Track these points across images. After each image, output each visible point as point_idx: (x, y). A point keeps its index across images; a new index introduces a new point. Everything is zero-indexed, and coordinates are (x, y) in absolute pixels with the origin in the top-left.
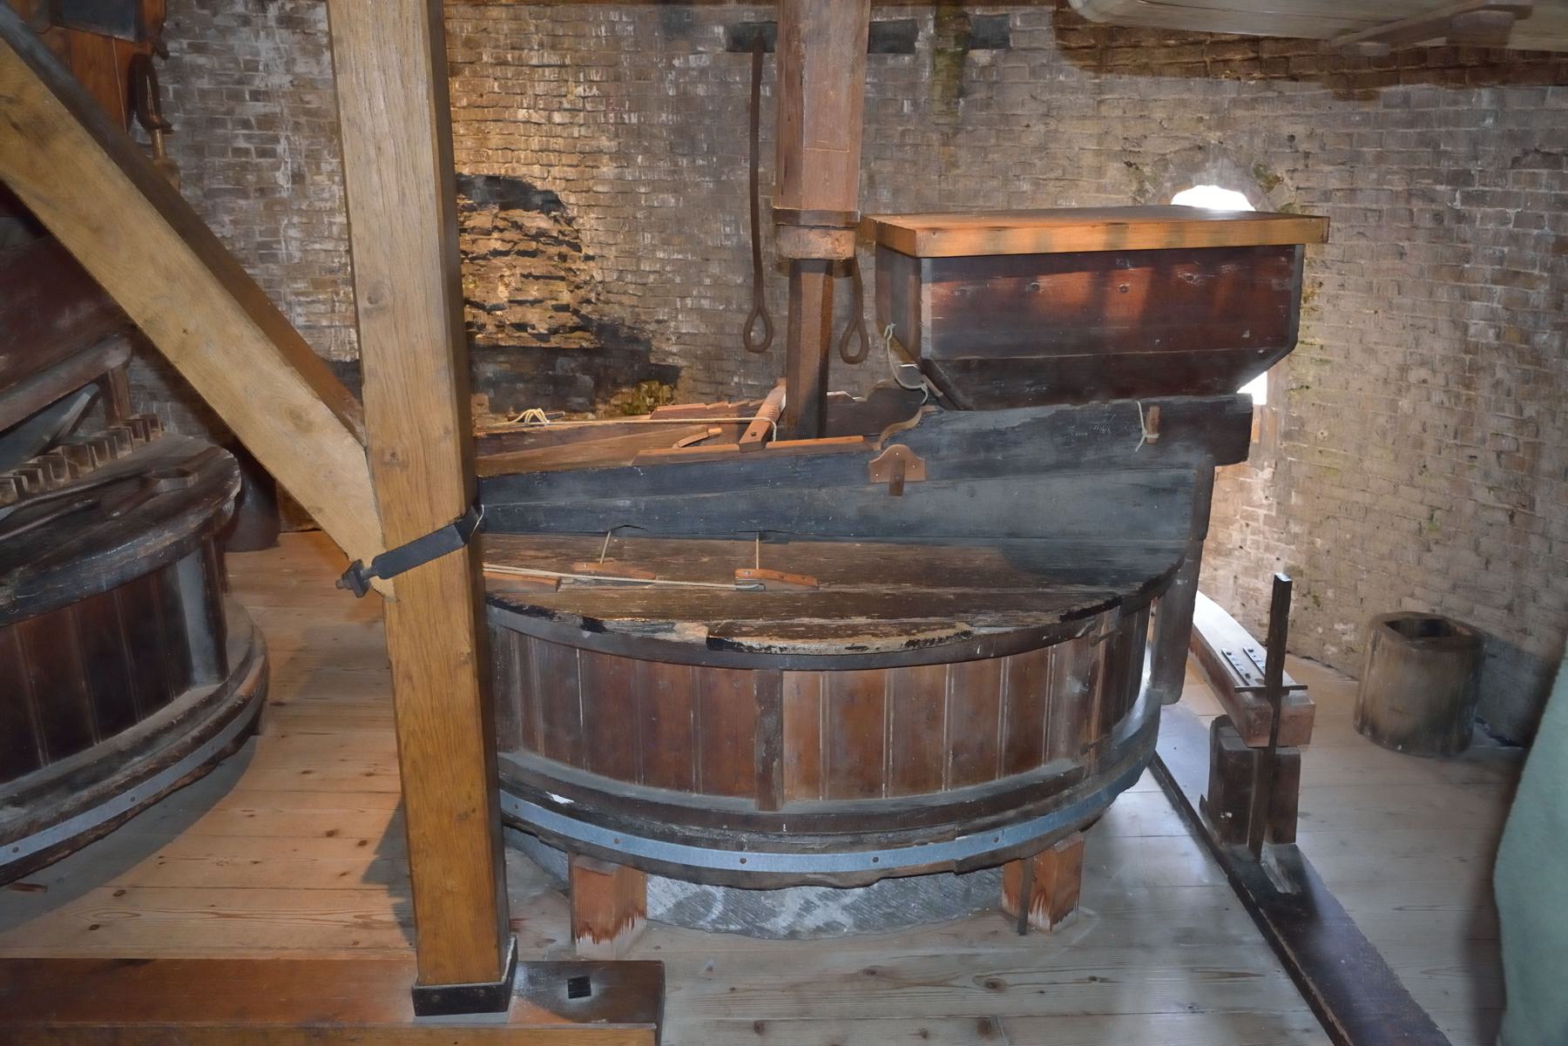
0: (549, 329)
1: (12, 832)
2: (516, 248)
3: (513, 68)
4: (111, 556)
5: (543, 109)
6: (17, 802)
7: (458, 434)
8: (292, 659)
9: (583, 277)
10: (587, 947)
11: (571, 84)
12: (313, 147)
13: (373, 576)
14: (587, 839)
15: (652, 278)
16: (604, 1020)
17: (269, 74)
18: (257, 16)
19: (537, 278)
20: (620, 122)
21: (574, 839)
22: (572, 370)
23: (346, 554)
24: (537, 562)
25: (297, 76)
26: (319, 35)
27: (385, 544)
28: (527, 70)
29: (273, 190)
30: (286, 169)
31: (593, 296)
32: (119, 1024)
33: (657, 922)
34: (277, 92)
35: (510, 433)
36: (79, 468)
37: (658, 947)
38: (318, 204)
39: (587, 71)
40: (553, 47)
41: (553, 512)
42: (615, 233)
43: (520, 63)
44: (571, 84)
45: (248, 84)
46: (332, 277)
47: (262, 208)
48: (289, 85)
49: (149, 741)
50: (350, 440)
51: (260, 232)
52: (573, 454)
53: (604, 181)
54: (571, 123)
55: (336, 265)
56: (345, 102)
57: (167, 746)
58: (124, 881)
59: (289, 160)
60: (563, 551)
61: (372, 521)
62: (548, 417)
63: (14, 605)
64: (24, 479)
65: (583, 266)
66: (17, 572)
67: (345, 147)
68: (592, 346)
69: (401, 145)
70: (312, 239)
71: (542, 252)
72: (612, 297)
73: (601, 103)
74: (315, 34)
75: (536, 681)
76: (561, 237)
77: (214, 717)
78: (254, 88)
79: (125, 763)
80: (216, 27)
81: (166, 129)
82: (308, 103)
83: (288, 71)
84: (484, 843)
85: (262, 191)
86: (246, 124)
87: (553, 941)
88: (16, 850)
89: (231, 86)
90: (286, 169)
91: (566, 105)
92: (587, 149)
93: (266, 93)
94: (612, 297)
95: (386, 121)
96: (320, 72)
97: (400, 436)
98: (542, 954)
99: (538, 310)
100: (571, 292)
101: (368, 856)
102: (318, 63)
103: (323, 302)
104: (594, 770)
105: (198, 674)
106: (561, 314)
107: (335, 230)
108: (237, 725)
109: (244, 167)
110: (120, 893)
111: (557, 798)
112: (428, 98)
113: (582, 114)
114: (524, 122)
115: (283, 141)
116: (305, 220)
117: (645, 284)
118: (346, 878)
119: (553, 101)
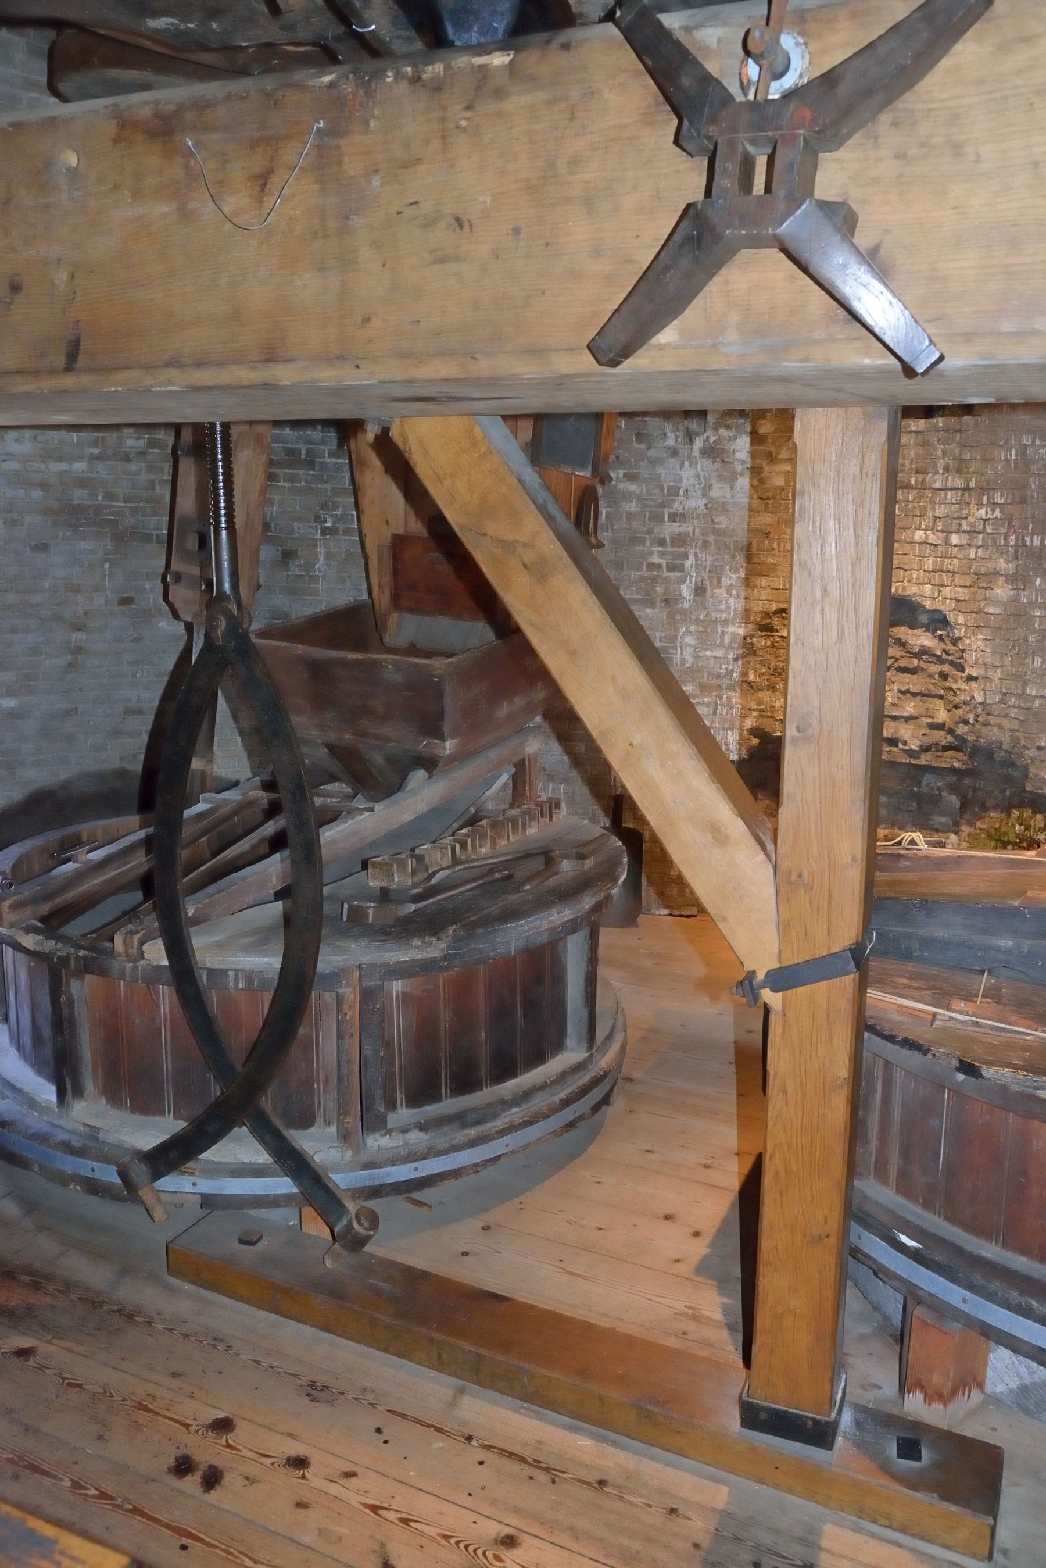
0: (921, 746)
1: (415, 1154)
2: (896, 665)
3: (915, 492)
4: (522, 926)
5: (941, 531)
6: (423, 1127)
7: (864, 863)
8: (643, 1038)
9: (963, 697)
10: (915, 1405)
11: (973, 507)
12: (716, 563)
13: (765, 987)
14: (933, 1290)
15: (1037, 703)
16: (935, 1495)
17: (687, 498)
18: (685, 448)
19: (914, 695)
20: (1021, 544)
21: (916, 1286)
22: (939, 789)
23: (742, 963)
24: (911, 992)
25: (711, 500)
26: (736, 463)
27: (780, 959)
28: (929, 493)
29: (677, 601)
30: (691, 582)
31: (971, 717)
32: (483, 1352)
33: (994, 1400)
34: (692, 514)
35: (886, 854)
36: (497, 840)
37: (994, 1429)
38: (714, 615)
39: (991, 493)
40: (959, 471)
41: (928, 943)
42: (1003, 655)
43: (923, 486)
44: (973, 507)
45: (669, 507)
46: (719, 682)
47: (665, 617)
48: (703, 507)
49: (526, 1096)
50: (762, 856)
51: (661, 638)
52: (950, 884)
53: (996, 603)
54: (968, 545)
55: (723, 671)
56: (799, 547)
57: (540, 1102)
58: (493, 1216)
59: (694, 575)
60: (938, 985)
61: (770, 936)
62: (926, 842)
63: (445, 958)
64: (458, 846)
65: (964, 686)
66: (451, 929)
67: (794, 587)
68: (964, 767)
69: (846, 589)
70: (705, 647)
71: (923, 669)
72: (992, 720)
73: (1003, 525)
74: (732, 463)
75: (897, 1114)
76: (944, 656)
77: (580, 1083)
78: (671, 511)
79: (506, 1111)
80: (649, 459)
81: (600, 545)
82: (718, 524)
83: (704, 495)
84: (833, 1272)
85: (667, 601)
86: (662, 542)
87: (880, 1388)
88: (416, 1169)
89: (654, 509)
90: (691, 582)
91: (965, 527)
92: (983, 570)
93: (683, 515)
94: (992, 720)
95: (835, 566)
96: (733, 496)
97: (808, 859)
98: (869, 1399)
99: (912, 727)
100: (949, 711)
101: (700, 1249)
102: (732, 488)
103: (708, 705)
104: (947, 1218)
105: (570, 1041)
106: (935, 732)
107: (727, 639)
108: (596, 1095)
109: (654, 580)
110: (486, 1228)
111: (904, 1239)
112: (878, 545)
113: (981, 536)
114: (920, 543)
115: (691, 557)
116: (701, 629)
117: (1029, 709)
118: (679, 1265)
119: (952, 524)
